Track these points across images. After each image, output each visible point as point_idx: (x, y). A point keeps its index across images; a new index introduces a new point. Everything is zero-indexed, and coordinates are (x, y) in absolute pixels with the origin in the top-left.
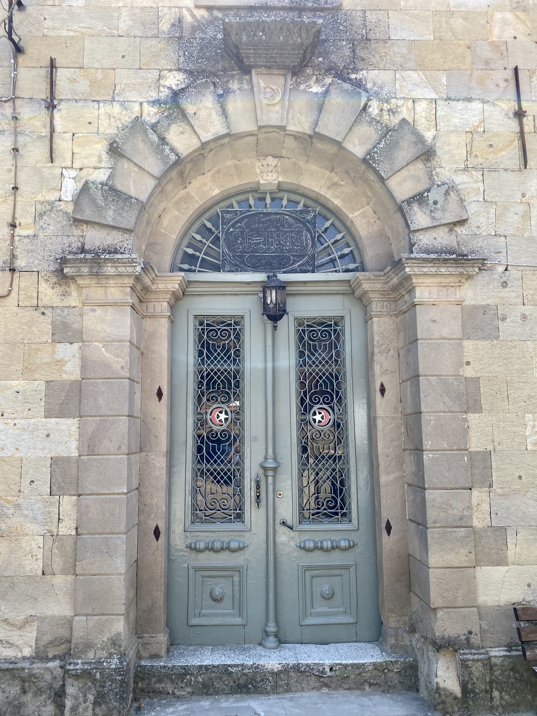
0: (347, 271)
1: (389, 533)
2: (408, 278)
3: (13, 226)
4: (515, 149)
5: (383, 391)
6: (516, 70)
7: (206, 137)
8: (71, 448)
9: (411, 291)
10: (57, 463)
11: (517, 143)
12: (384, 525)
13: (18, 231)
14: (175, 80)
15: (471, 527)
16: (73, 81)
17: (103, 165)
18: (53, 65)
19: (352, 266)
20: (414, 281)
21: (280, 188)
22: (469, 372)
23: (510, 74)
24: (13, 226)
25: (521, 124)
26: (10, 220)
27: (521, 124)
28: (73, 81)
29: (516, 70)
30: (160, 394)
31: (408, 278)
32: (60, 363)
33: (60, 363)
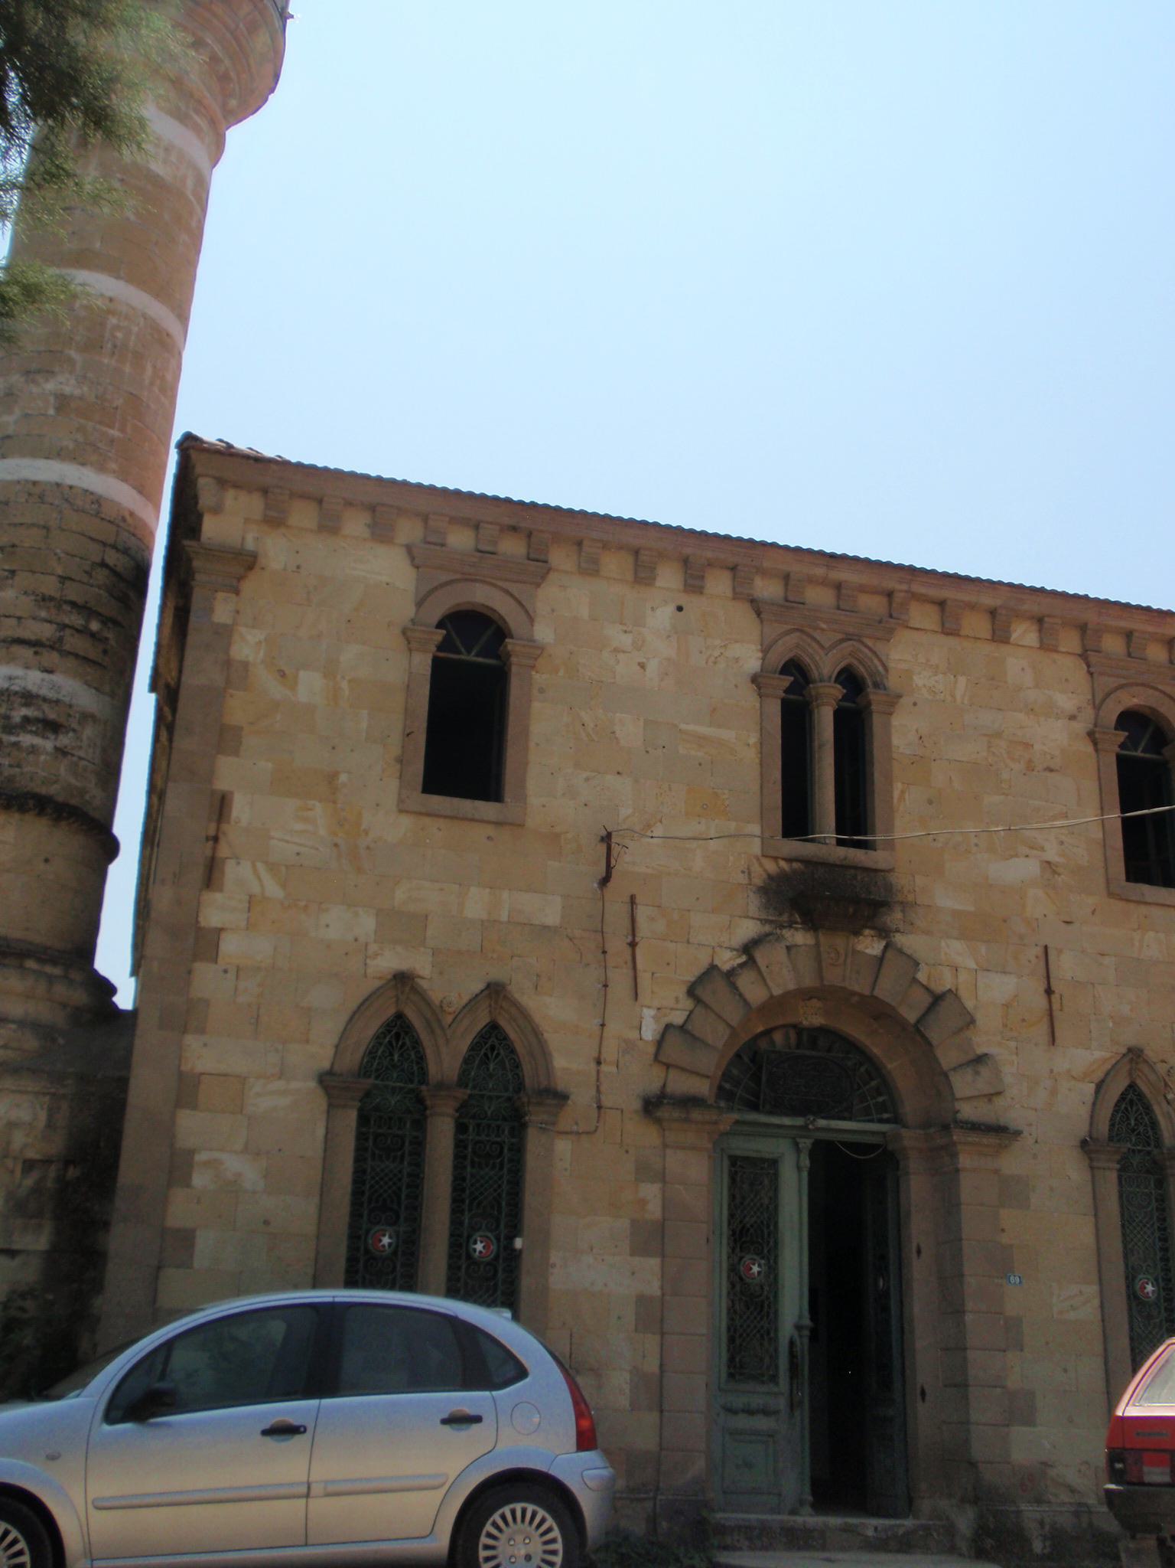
0: (881, 1121)
1: (923, 1399)
2: (954, 1144)
3: (599, 1063)
4: (1044, 1027)
5: (919, 1252)
6: (1046, 947)
7: (777, 991)
8: (654, 1288)
9: (954, 1156)
10: (642, 1300)
11: (1046, 1020)
12: (918, 1391)
13: (604, 1068)
14: (748, 929)
15: (1003, 1387)
16: (652, 919)
17: (680, 1006)
18: (633, 900)
19: (886, 1116)
20: (959, 1147)
21: (821, 1030)
22: (1004, 1239)
23: (1040, 951)
24: (599, 1063)
25: (1050, 1002)
26: (595, 1054)
27: (1050, 1002)
28: (652, 919)
29: (1046, 947)
30: (919, 1252)
31: (954, 1144)
32: (643, 1203)
33: (643, 1203)
